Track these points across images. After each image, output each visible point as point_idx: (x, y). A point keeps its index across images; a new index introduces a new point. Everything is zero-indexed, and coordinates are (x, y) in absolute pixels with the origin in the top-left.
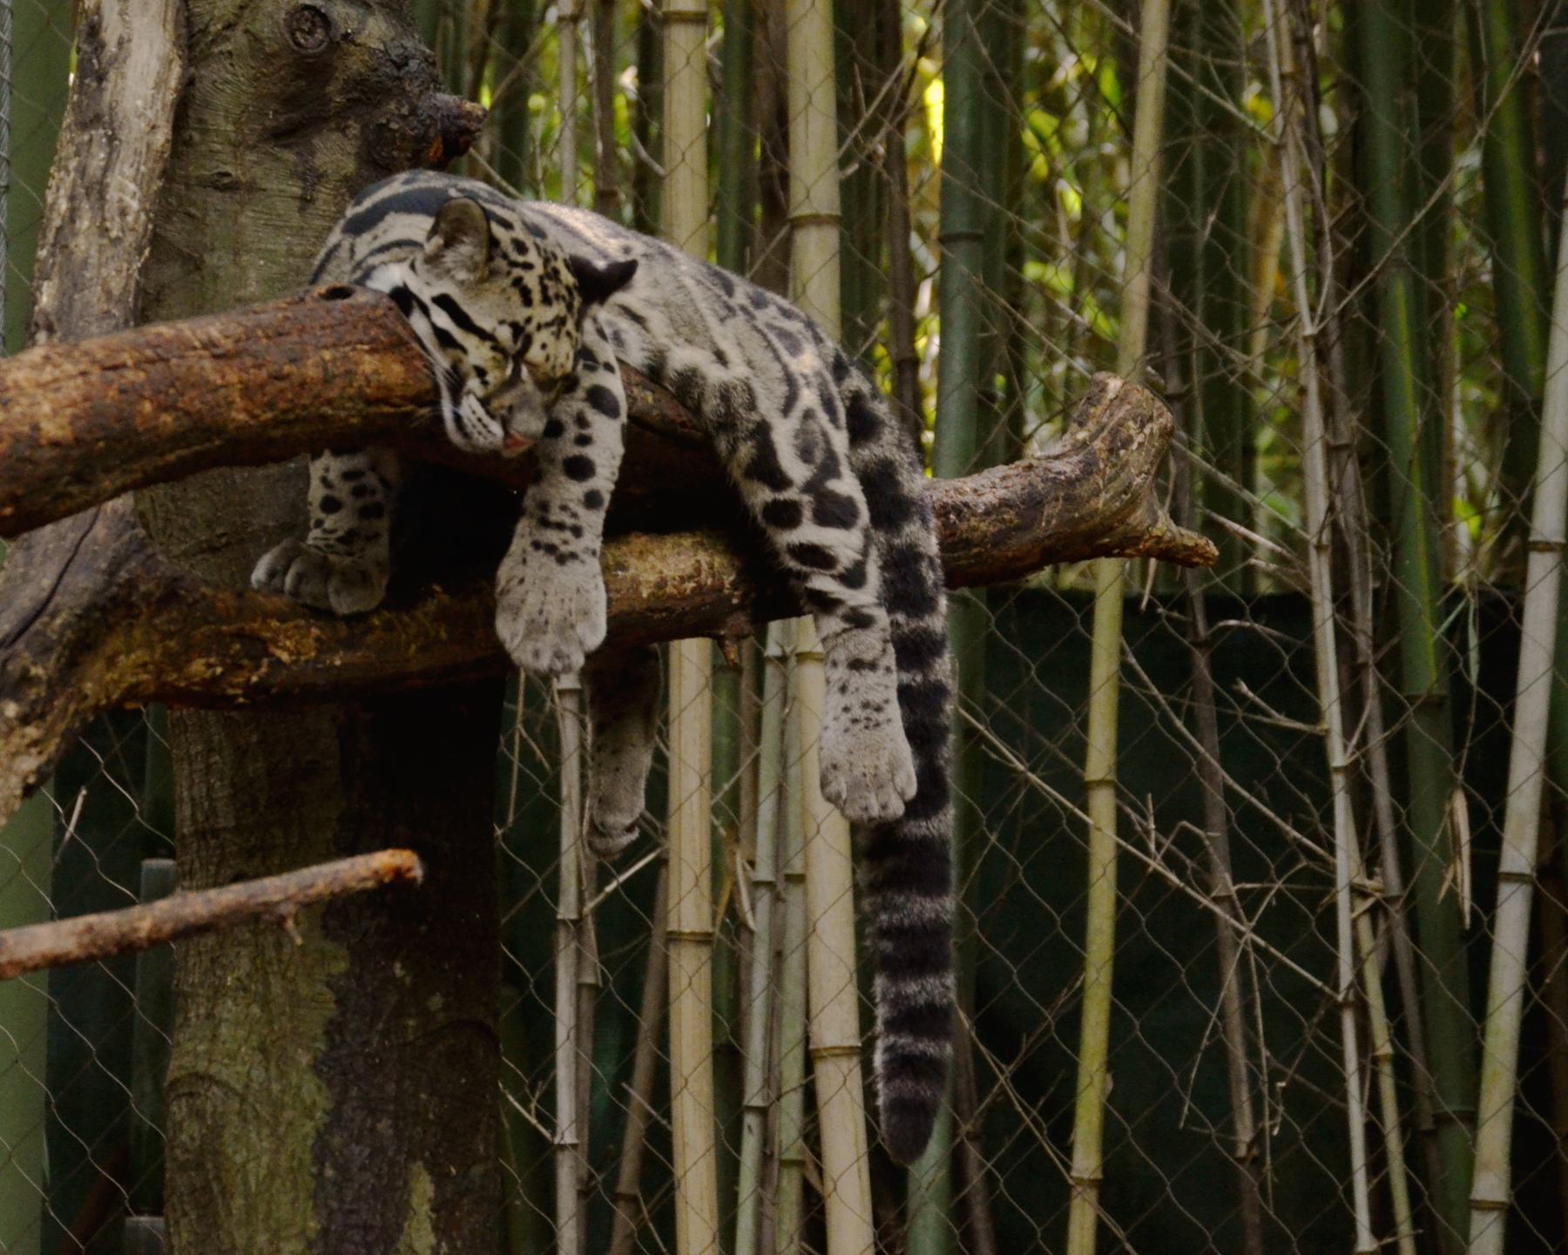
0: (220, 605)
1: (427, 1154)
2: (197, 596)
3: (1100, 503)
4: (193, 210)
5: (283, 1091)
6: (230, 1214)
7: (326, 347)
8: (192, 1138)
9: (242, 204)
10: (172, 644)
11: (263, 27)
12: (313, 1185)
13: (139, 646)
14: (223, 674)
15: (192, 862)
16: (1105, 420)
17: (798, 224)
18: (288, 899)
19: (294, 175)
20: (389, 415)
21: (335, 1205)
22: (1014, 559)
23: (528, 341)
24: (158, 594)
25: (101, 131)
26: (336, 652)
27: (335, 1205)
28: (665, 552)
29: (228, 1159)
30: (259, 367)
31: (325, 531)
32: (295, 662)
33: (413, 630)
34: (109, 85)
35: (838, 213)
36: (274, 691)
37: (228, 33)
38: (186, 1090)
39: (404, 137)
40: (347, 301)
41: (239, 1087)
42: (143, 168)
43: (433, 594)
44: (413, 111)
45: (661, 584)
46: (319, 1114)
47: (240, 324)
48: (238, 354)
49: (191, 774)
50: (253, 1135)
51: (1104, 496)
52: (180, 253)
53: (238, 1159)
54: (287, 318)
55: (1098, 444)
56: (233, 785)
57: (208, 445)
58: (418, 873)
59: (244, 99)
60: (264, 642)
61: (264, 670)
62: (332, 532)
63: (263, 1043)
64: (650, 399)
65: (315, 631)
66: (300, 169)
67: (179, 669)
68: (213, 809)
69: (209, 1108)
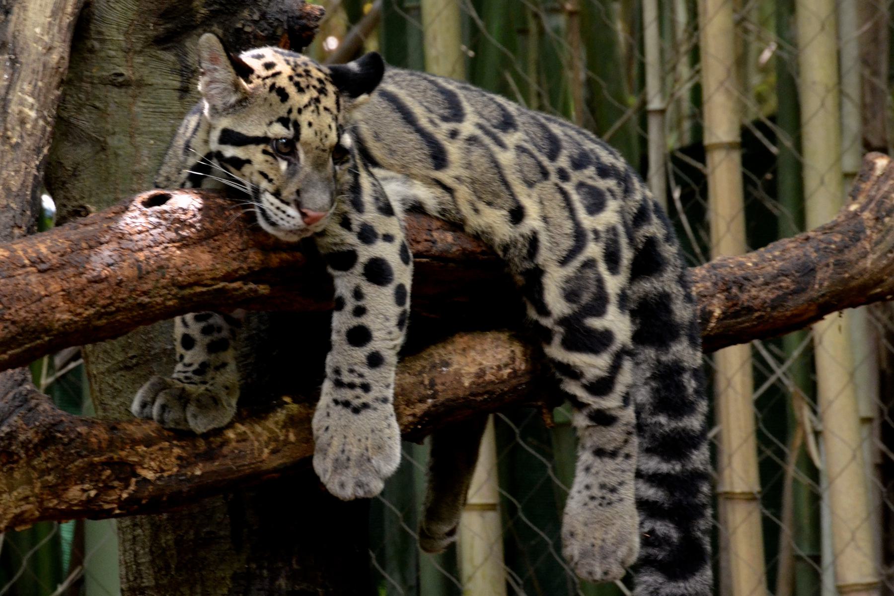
0: (93, 440)
3: (868, 263)
4: (97, 104)
9: (134, 97)
10: (50, 478)
13: (21, 484)
14: (96, 495)
16: (873, 193)
19: (173, 71)
20: (202, 293)
22: (793, 316)
23: (297, 126)
24: (36, 440)
25: (7, 56)
26: (196, 464)
28: (486, 347)
31: (185, 365)
32: (159, 479)
33: (265, 436)
34: (13, 18)
36: (144, 502)
42: (40, 84)
43: (282, 405)
44: (263, 16)
45: (481, 373)
47: (67, 239)
48: (62, 266)
51: (871, 257)
52: (90, 137)
55: (866, 215)
56: (152, 552)
57: (39, 341)
59: (130, 15)
60: (132, 466)
61: (132, 488)
62: (190, 365)
65: (177, 451)
66: (178, 67)
67: (58, 496)
68: (139, 571)
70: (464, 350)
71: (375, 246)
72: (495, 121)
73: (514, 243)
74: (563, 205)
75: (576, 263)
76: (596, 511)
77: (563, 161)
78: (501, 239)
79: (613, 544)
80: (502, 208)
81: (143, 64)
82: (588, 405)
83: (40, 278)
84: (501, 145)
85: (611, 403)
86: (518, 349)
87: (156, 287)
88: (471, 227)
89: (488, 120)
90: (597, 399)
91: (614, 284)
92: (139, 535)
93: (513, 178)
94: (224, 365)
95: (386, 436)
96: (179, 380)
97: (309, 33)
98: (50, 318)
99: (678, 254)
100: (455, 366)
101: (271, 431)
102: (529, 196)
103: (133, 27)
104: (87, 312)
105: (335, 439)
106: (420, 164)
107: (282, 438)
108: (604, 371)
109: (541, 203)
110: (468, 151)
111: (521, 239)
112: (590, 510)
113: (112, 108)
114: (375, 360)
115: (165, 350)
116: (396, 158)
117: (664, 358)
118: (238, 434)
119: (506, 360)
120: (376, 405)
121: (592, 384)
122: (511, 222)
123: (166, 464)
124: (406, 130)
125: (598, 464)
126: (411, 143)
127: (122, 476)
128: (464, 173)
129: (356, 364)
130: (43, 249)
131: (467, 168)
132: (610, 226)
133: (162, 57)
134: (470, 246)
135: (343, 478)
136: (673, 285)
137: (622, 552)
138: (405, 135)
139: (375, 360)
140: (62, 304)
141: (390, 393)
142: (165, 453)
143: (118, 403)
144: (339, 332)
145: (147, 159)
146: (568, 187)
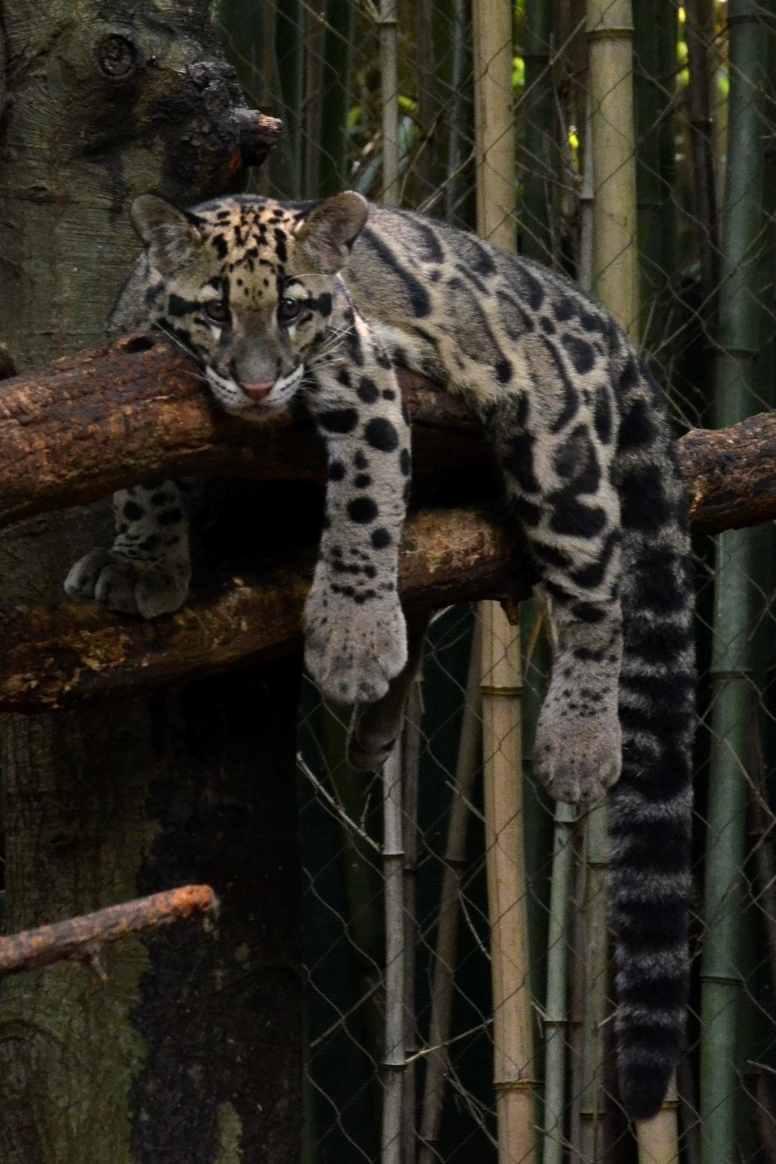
0: (35, 621)
1: (235, 1095)
2: (13, 615)
4: (12, 222)
5: (101, 1041)
6: (54, 1154)
7: (128, 402)
8: (19, 1081)
9: (57, 216)
11: (74, 56)
12: (129, 1128)
14: (37, 686)
15: (17, 819)
17: (594, 37)
18: (93, 939)
19: (104, 187)
21: (149, 1147)
27: (149, 1147)
28: (450, 527)
29: (51, 1102)
30: (65, 429)
31: (129, 537)
32: (105, 670)
33: (216, 623)
35: (631, 27)
36: (86, 696)
37: (43, 58)
38: (13, 1035)
39: (205, 153)
40: (147, 353)
41: (60, 1036)
44: (214, 128)
45: (447, 559)
46: (135, 1062)
47: (47, 386)
48: (45, 419)
49: (15, 738)
50: (74, 1081)
53: (61, 1103)
54: (91, 375)
57: (18, 506)
58: (215, 903)
60: (77, 654)
61: (76, 679)
62: (136, 538)
63: (83, 995)
64: (433, 400)
65: (124, 638)
66: (111, 182)
69: (34, 1054)
70: (428, 530)
71: (376, 405)
72: (473, 262)
73: (502, 404)
74: (551, 361)
75: (568, 430)
76: (576, 721)
77: (546, 310)
78: (488, 400)
79: (595, 761)
80: (489, 363)
81: (68, 178)
82: (575, 597)
83: (23, 432)
84: (482, 288)
85: (599, 595)
86: (487, 531)
87: (142, 447)
88: (454, 384)
89: (468, 261)
90: (585, 591)
91: (605, 454)
92: (37, 732)
93: (497, 329)
94: (176, 540)
95: (393, 629)
96: (122, 554)
97: (265, 151)
98: (35, 478)
99: (666, 421)
100: (420, 550)
101: (223, 619)
102: (514, 350)
103: (60, 134)
104: (71, 474)
105: (335, 633)
106: (399, 310)
107: (234, 627)
108: (594, 558)
109: (527, 358)
110: (452, 296)
111: (510, 400)
112: (570, 720)
113: (30, 228)
114: (380, 540)
115: (82, 515)
116: (374, 302)
117: (652, 543)
118: (188, 620)
119: (473, 544)
120: (382, 593)
121: (580, 572)
122: (499, 379)
123: (112, 653)
124: (384, 269)
125: (580, 667)
126: (391, 285)
127: (65, 665)
128: (449, 321)
129: (359, 544)
130: (23, 399)
131: (450, 315)
132: (600, 386)
133: (91, 170)
134: (453, 409)
135: (345, 680)
136: (662, 458)
137: (604, 770)
138: (384, 275)
139: (380, 540)
140: (45, 463)
141: (393, 578)
142: (111, 639)
143: (18, 576)
144: (337, 505)
145: (68, 289)
146: (555, 340)
